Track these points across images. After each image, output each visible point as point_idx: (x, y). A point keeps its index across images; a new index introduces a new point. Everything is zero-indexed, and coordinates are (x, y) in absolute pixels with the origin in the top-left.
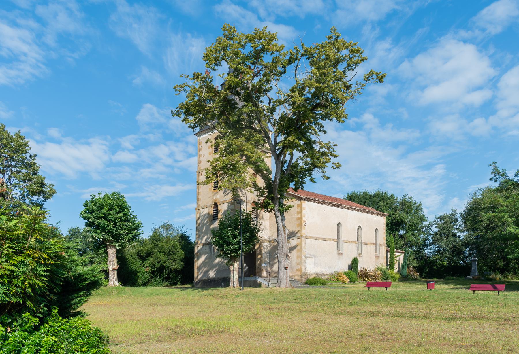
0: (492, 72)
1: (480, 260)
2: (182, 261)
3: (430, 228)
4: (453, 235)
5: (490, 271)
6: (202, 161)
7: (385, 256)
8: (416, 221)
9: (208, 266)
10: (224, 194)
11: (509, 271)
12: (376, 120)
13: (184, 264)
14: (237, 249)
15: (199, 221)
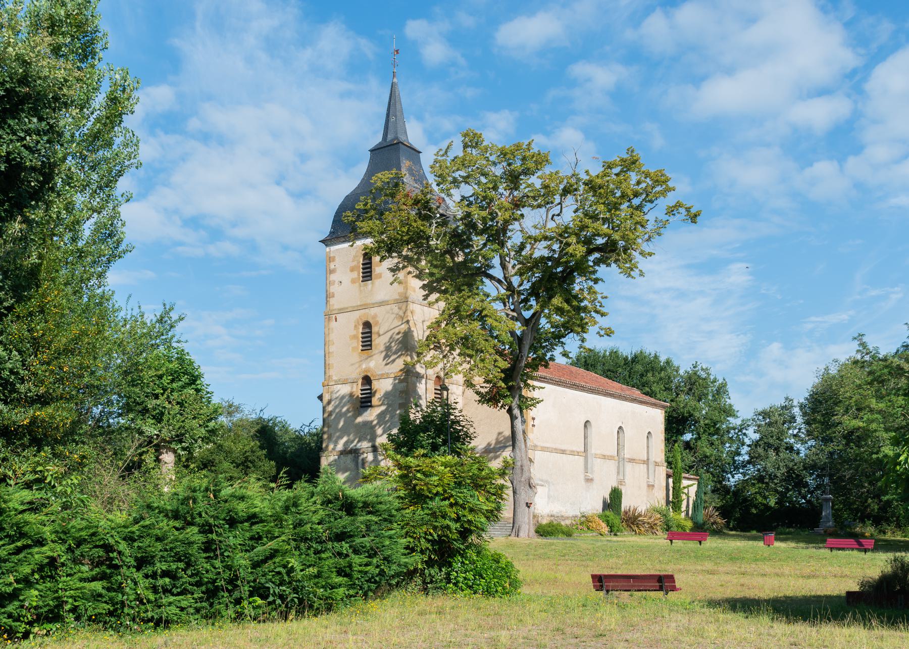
0: (849, 58)
1: (837, 498)
3: (744, 431)
4: (787, 449)
5: (855, 520)
7: (665, 485)
8: (716, 416)
11: (888, 522)
15: (330, 408)
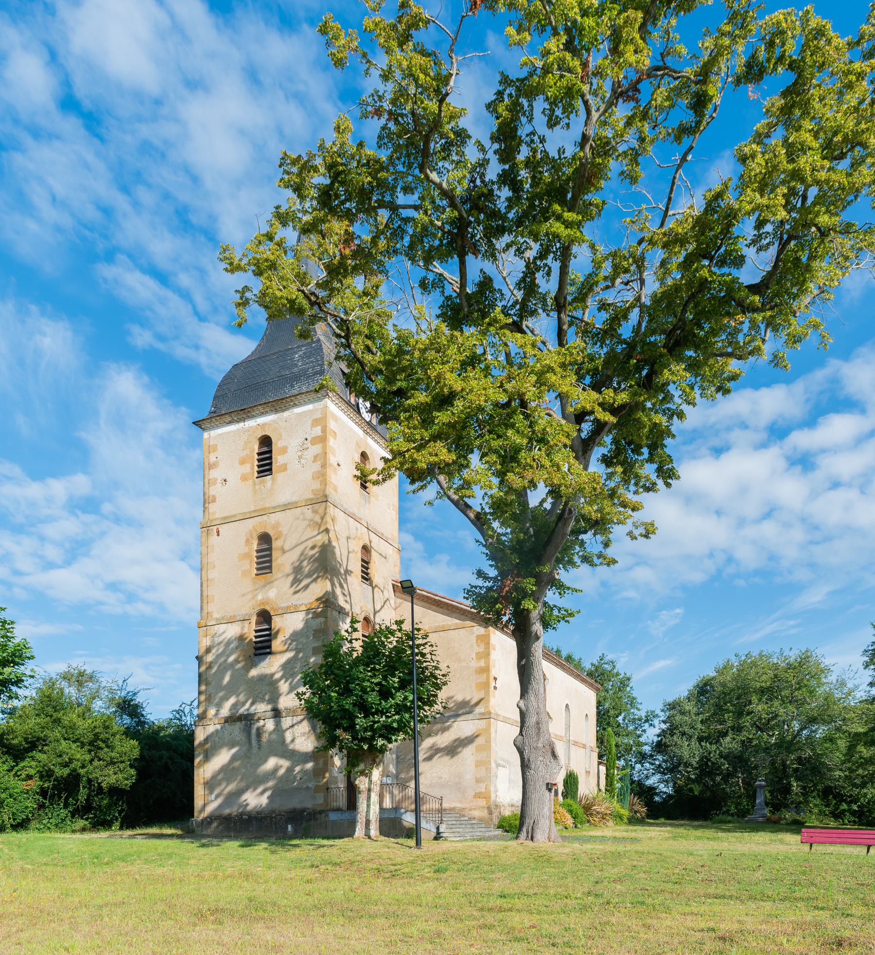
2: (131, 766)
6: (217, 496)
9: (242, 780)
10: (292, 586)
12: (420, 546)
13: (137, 774)
14: (395, 725)
